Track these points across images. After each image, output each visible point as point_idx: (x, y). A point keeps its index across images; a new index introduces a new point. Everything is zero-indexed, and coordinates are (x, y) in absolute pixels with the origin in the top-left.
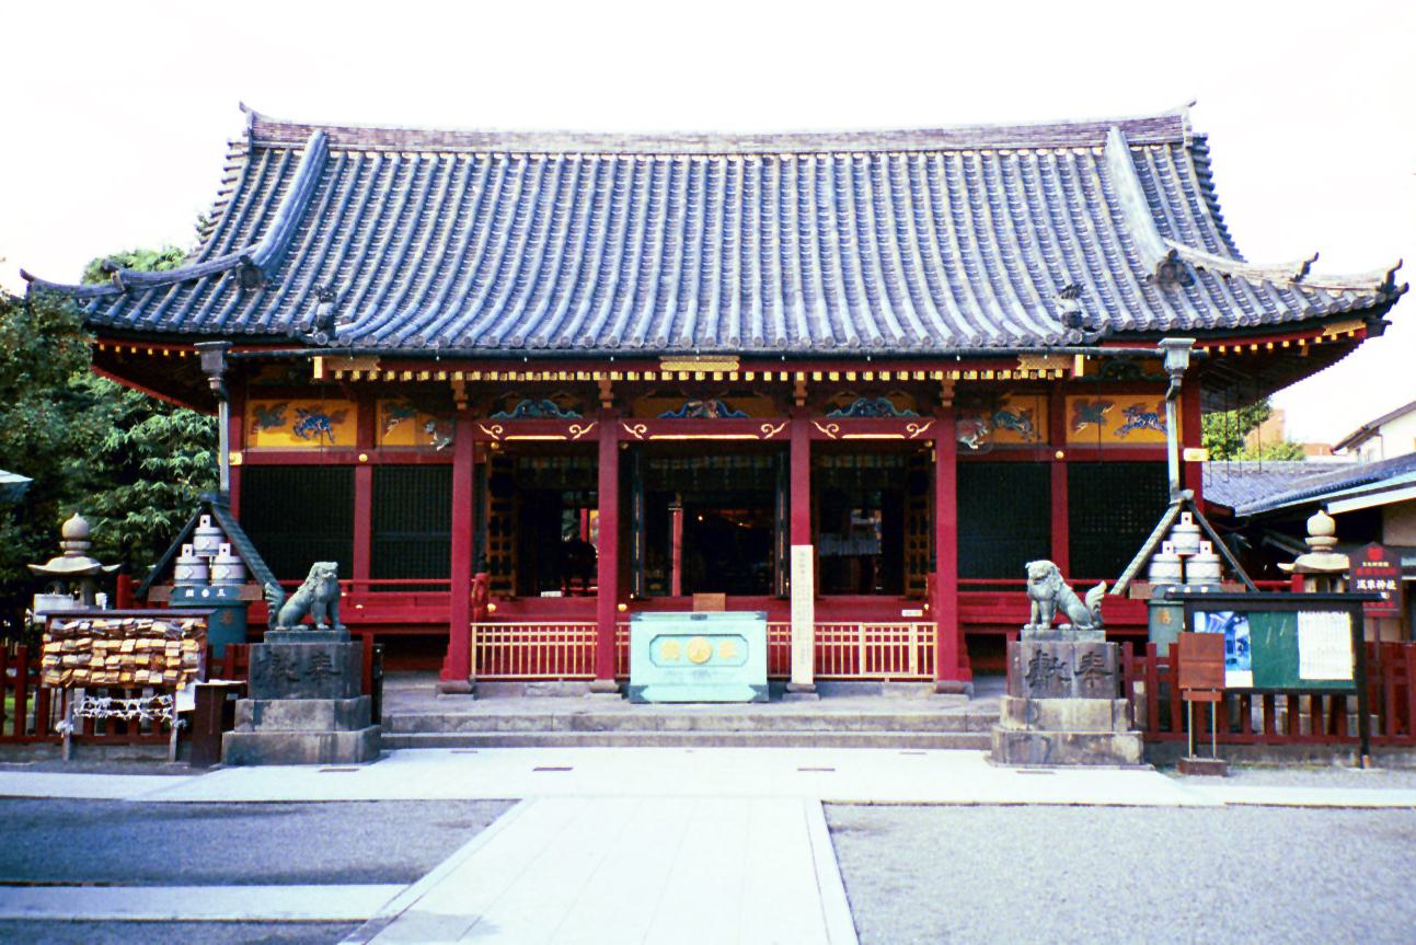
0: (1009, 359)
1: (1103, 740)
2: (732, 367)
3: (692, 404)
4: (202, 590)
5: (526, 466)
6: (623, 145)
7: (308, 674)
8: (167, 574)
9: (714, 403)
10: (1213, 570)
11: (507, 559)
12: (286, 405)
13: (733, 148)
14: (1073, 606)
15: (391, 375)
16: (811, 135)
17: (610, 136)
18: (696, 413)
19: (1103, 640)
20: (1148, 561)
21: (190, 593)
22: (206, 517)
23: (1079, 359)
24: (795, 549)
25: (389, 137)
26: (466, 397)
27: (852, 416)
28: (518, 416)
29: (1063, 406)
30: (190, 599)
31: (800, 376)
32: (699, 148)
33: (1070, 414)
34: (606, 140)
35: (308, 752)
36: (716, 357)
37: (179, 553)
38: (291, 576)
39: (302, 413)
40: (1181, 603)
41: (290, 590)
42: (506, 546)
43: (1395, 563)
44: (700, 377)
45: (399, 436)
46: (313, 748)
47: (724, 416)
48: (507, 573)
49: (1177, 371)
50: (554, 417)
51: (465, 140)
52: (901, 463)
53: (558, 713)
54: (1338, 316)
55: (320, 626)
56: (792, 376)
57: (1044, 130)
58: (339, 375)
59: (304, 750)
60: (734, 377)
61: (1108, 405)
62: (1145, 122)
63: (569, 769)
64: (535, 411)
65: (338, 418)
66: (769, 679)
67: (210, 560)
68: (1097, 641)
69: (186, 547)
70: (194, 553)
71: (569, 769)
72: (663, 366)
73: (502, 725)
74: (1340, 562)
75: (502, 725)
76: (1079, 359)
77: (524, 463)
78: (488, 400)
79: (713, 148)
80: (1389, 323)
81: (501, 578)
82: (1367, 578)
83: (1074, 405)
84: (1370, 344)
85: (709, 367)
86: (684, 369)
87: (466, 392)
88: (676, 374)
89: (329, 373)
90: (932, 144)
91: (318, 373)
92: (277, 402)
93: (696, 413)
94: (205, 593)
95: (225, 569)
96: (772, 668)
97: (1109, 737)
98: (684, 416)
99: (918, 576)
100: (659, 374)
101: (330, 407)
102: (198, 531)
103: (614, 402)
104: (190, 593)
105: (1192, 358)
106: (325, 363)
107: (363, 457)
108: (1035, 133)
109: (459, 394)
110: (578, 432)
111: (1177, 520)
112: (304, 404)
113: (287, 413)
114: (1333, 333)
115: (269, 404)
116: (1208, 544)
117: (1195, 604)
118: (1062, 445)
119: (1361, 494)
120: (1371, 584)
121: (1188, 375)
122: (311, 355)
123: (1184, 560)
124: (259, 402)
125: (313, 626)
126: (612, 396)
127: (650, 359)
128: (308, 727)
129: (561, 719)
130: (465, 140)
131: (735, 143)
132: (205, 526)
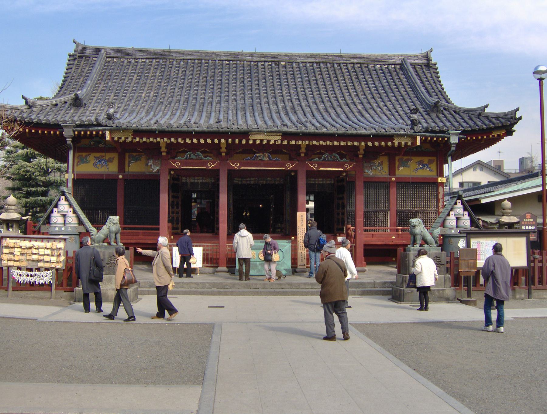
0: (390, 137)
1: (441, 292)
2: (279, 138)
3: (257, 155)
4: (62, 227)
5: (185, 181)
6: (220, 57)
7: (108, 264)
8: (48, 221)
9: (267, 154)
10: (468, 223)
11: (177, 218)
12: (90, 155)
13: (262, 59)
14: (429, 237)
15: (137, 139)
16: (293, 55)
17: (215, 53)
18: (259, 158)
19: (440, 251)
20: (444, 221)
21: (57, 229)
22: (63, 197)
23: (418, 138)
24: (299, 214)
25: (130, 52)
26: (166, 150)
27: (322, 161)
28: (186, 159)
29: (395, 160)
30: (57, 231)
31: (223, 141)
32: (249, 59)
33: (397, 164)
34: (214, 55)
35: (110, 297)
36: (272, 134)
37: (52, 212)
38: (98, 223)
39: (96, 158)
40: (465, 235)
41: (98, 229)
42: (177, 213)
43: (535, 220)
44: (265, 142)
45: (135, 167)
46: (112, 295)
47: (271, 160)
48: (177, 224)
49: (454, 144)
50: (201, 159)
51: (159, 54)
52: (332, 182)
53: (208, 281)
54: (497, 128)
55: (113, 243)
56: (219, 141)
57: (379, 58)
58: (116, 139)
59: (108, 296)
60: (279, 142)
61: (410, 160)
62: (415, 57)
63: (223, 307)
64: (193, 156)
65: (110, 160)
66: (292, 267)
67: (65, 214)
68: (437, 251)
69: (55, 209)
70: (455, 215)
71: (223, 307)
72: (250, 137)
73: (185, 286)
74: (514, 219)
75: (185, 286)
76: (418, 138)
77: (184, 179)
78: (174, 150)
79: (255, 59)
80: (515, 131)
81: (175, 225)
82: (525, 225)
83: (399, 160)
84: (506, 139)
85: (261, 137)
86: (258, 138)
87: (166, 148)
88: (254, 141)
89: (113, 138)
90: (338, 60)
91: (108, 137)
92: (87, 153)
93: (259, 158)
94: (63, 229)
95: (72, 219)
96: (292, 264)
97: (443, 290)
98: (254, 160)
99: (340, 226)
100: (248, 141)
101: (108, 156)
102: (60, 203)
103: (167, 153)
104: (57, 229)
105: (459, 139)
106: (111, 133)
107: (120, 177)
108: (376, 58)
109: (223, 149)
110: (211, 166)
111: (456, 203)
112: (98, 155)
113: (89, 158)
114: (495, 134)
115: (84, 154)
116: (466, 213)
117: (472, 235)
118: (394, 174)
119: (492, 196)
120: (527, 228)
121: (458, 145)
122: (105, 130)
123: (458, 219)
124: (80, 154)
125: (109, 244)
126: (226, 151)
127: (245, 134)
128: (109, 287)
129: (209, 283)
130: (159, 54)
131: (263, 57)
132: (63, 201)
